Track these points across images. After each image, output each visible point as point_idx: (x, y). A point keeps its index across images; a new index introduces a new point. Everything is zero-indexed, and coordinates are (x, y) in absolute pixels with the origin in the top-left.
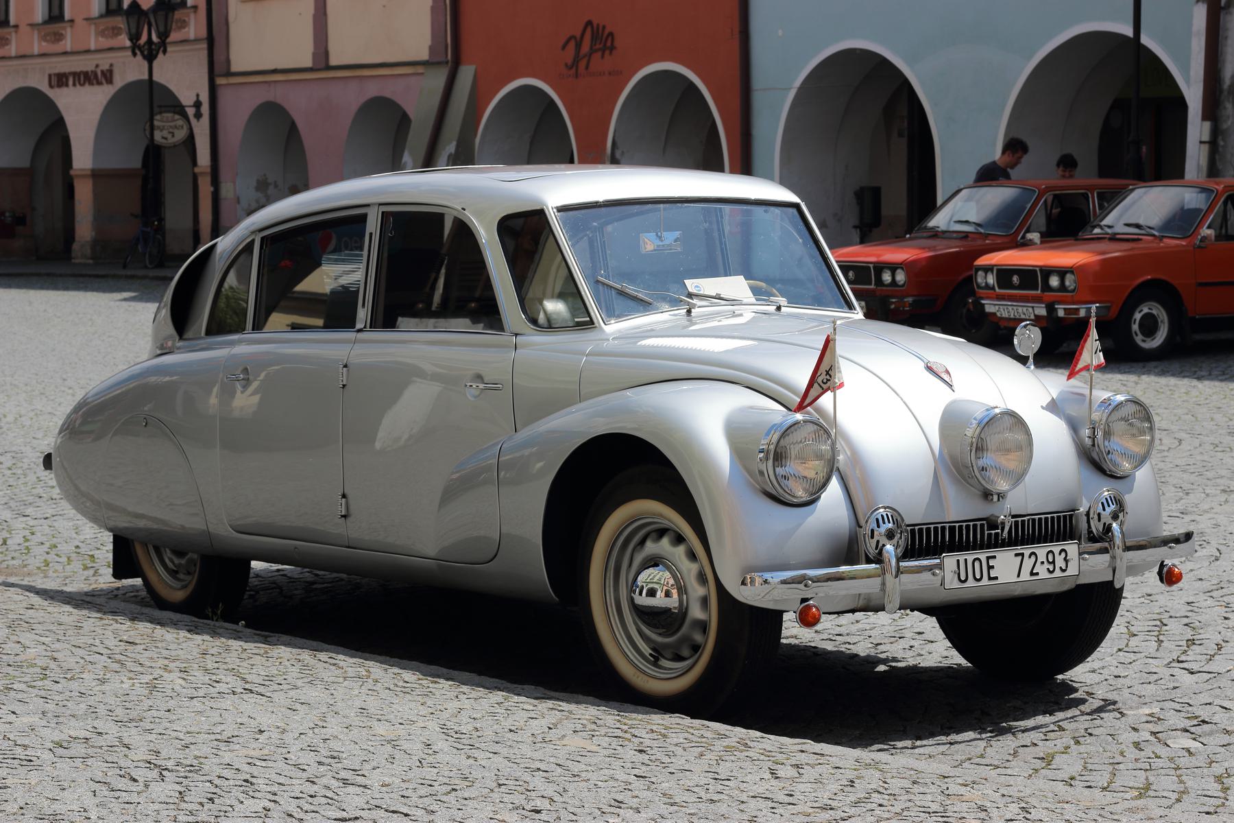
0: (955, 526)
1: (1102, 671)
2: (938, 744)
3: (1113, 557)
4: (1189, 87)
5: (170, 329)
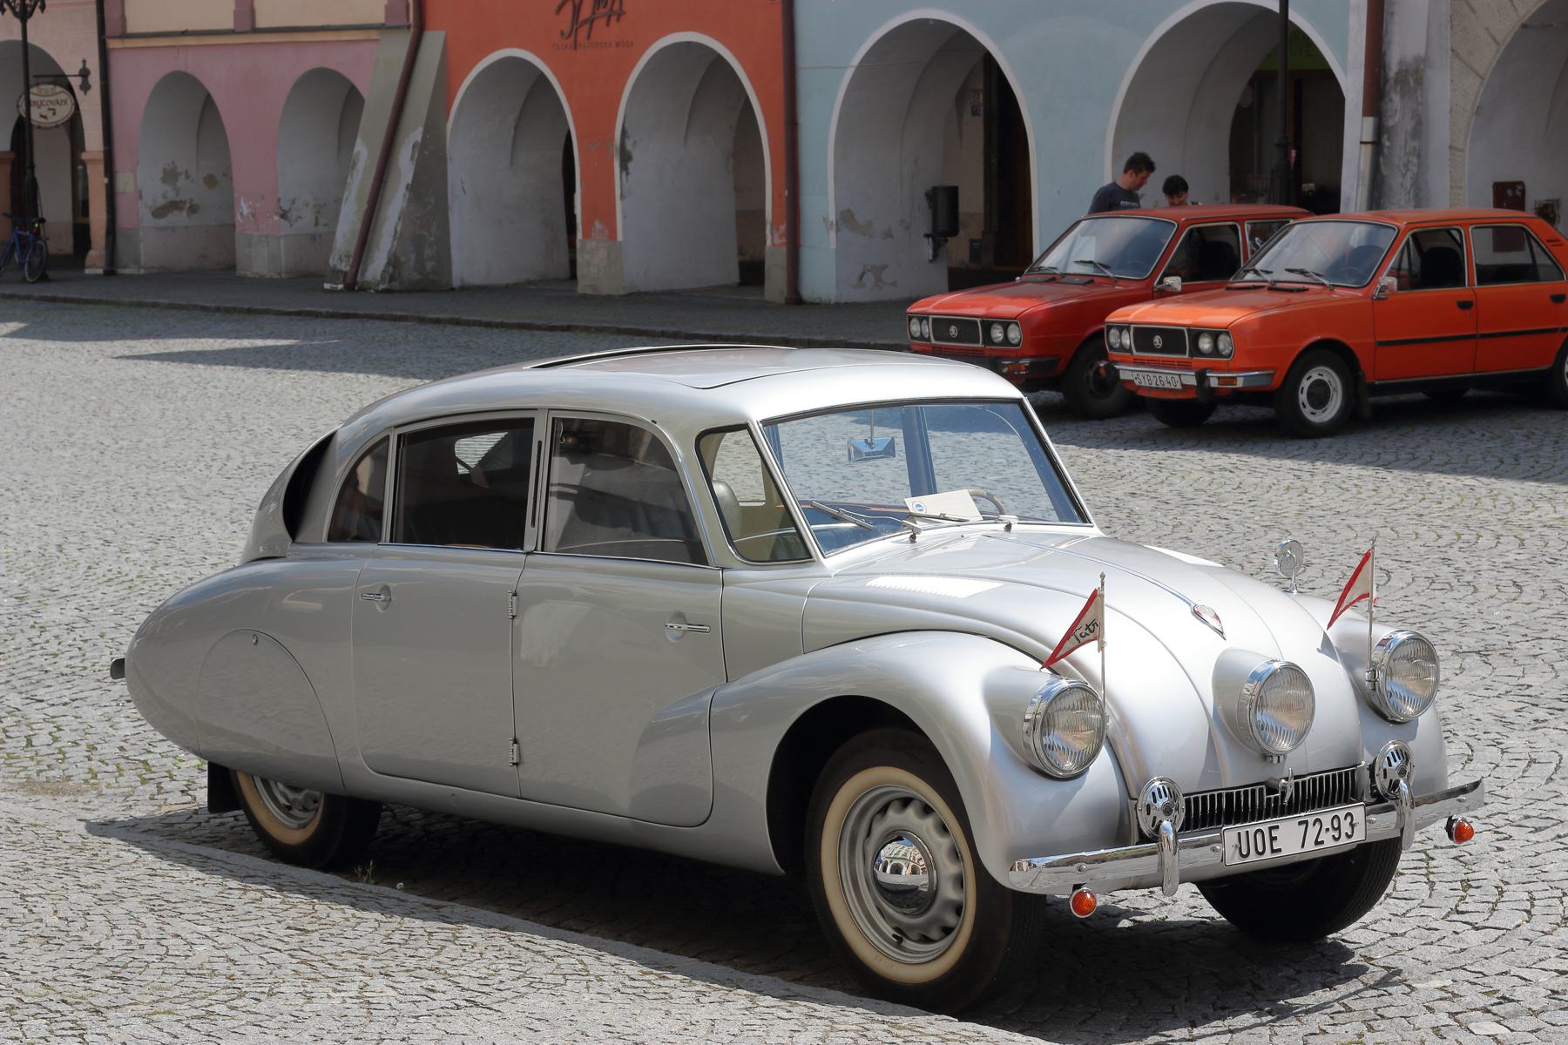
0: (1232, 793)
1: (1375, 927)
2: (1218, 1033)
3: (1401, 815)
4: (1345, 73)
5: (281, 529)
